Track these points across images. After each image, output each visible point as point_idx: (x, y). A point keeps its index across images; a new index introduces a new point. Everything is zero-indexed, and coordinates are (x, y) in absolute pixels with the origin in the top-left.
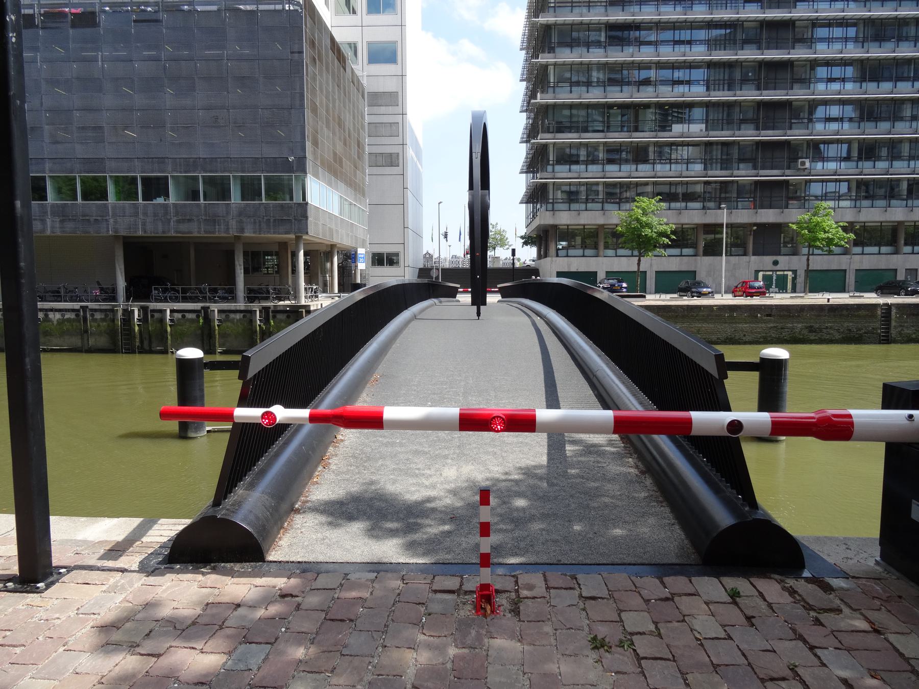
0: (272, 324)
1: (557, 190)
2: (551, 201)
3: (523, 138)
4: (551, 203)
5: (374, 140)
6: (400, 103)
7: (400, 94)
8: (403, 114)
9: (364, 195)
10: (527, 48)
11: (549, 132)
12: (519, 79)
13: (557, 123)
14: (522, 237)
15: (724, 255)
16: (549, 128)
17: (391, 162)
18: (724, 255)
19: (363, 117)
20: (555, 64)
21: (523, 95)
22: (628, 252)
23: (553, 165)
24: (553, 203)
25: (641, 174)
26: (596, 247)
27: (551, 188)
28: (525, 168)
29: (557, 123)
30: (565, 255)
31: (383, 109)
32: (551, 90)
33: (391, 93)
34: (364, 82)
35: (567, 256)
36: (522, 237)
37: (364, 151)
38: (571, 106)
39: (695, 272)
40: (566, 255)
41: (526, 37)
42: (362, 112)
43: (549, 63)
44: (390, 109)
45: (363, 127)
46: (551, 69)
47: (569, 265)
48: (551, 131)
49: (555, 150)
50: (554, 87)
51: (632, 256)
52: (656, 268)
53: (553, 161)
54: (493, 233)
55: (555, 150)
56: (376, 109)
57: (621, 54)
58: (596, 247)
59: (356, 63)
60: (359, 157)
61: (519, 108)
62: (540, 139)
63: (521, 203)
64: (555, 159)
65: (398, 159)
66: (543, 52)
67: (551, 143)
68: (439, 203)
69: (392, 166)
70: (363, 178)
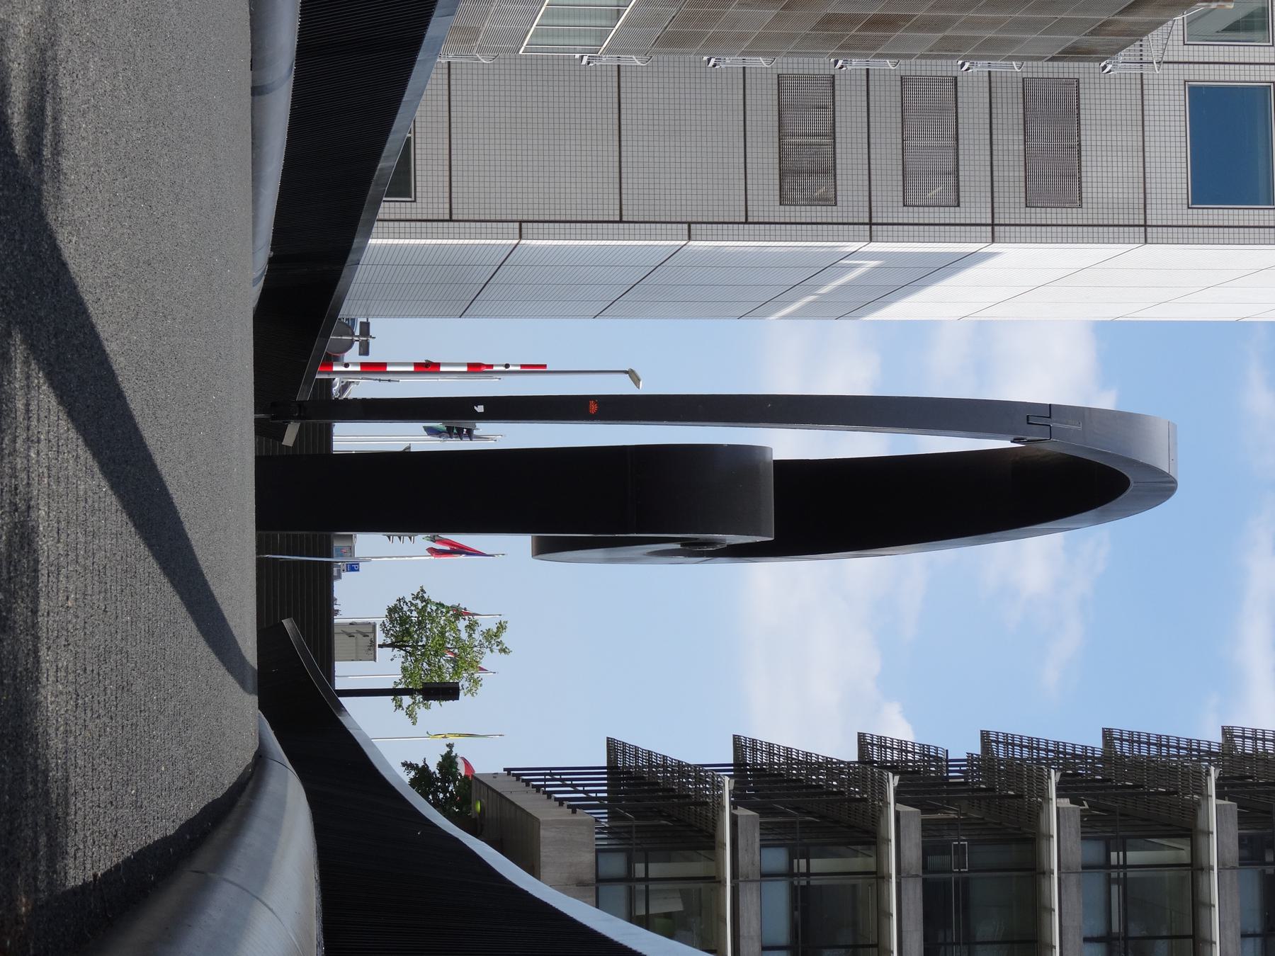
1: (685, 895)
2: (639, 869)
3: (754, 750)
4: (630, 868)
5: (887, 100)
6: (1039, 215)
7: (1073, 215)
8: (994, 228)
9: (672, 40)
10: (1110, 756)
11: (927, 851)
12: (992, 727)
13: (965, 884)
14: (448, 762)
16: (944, 849)
17: (799, 172)
19: (990, 49)
20: (1196, 868)
21: (1061, 738)
23: (790, 874)
24: (629, 878)
27: (696, 868)
28: (762, 758)
29: (965, 884)
31: (1011, 142)
32: (1094, 852)
33: (1076, 176)
34: (1120, 66)
36: (448, 762)
37: (849, 48)
41: (1173, 751)
42: (1012, 43)
43: (1202, 840)
44: (1011, 173)
45: (948, 49)
46: (1174, 852)
48: (935, 860)
49: (848, 881)
50: (1107, 865)
53: (808, 874)
54: (464, 635)
55: (848, 881)
56: (1011, 113)
59: (1194, 35)
60: (829, 21)
61: (999, 725)
62: (897, 814)
63: (612, 746)
64: (815, 882)
65: (812, 202)
66: (1243, 820)
67: (880, 859)
68: (631, 373)
69: (782, 175)
70: (741, 38)
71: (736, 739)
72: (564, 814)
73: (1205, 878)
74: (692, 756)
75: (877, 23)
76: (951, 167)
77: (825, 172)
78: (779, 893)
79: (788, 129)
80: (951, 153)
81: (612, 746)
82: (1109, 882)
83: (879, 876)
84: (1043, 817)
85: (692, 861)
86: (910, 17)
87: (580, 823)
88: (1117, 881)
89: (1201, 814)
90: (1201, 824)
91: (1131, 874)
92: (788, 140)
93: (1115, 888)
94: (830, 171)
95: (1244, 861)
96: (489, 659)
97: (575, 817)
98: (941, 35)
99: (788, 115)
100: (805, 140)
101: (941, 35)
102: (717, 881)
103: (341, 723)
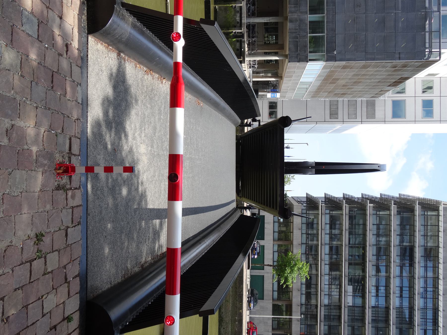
0: (233, 40)
1: (314, 216)
3: (346, 195)
4: (307, 212)
5: (346, 104)
6: (369, 120)
7: (374, 120)
9: (312, 97)
11: (349, 211)
13: (355, 216)
15: (273, 316)
18: (273, 316)
19: (360, 97)
20: (390, 215)
22: (276, 259)
24: (306, 213)
25: (323, 267)
26: (279, 239)
27: (316, 212)
29: (355, 216)
30: (275, 221)
31: (365, 109)
34: (382, 98)
35: (274, 222)
37: (339, 97)
38: (365, 225)
39: (263, 299)
40: (275, 221)
43: (391, 211)
44: (365, 114)
46: (387, 212)
47: (268, 223)
48: (351, 212)
50: (377, 214)
51: (273, 261)
52: (266, 275)
54: (289, 177)
56: (365, 105)
57: (395, 255)
58: (279, 239)
60: (335, 94)
64: (333, 215)
66: (398, 208)
68: (307, 143)
70: (324, 96)
71: (343, 193)
72: (297, 204)
73: (391, 216)
74: (336, 196)
75: (342, 94)
76: (356, 113)
77: (337, 114)
78: (328, 216)
79: (331, 108)
80: (356, 111)
81: (325, 194)
82: (377, 216)
83: (342, 214)
84: (367, 207)
85: (349, 220)
86: (347, 93)
87: (300, 205)
88: (378, 216)
89: (391, 207)
90: (391, 209)
91: (380, 215)
92: (331, 110)
93: (377, 217)
94: (337, 114)
95: (397, 214)
96: (292, 180)
97: (299, 205)
98: (352, 95)
99: (331, 106)
100: (334, 110)
101: (352, 95)
102: (319, 214)
103: (239, 255)
